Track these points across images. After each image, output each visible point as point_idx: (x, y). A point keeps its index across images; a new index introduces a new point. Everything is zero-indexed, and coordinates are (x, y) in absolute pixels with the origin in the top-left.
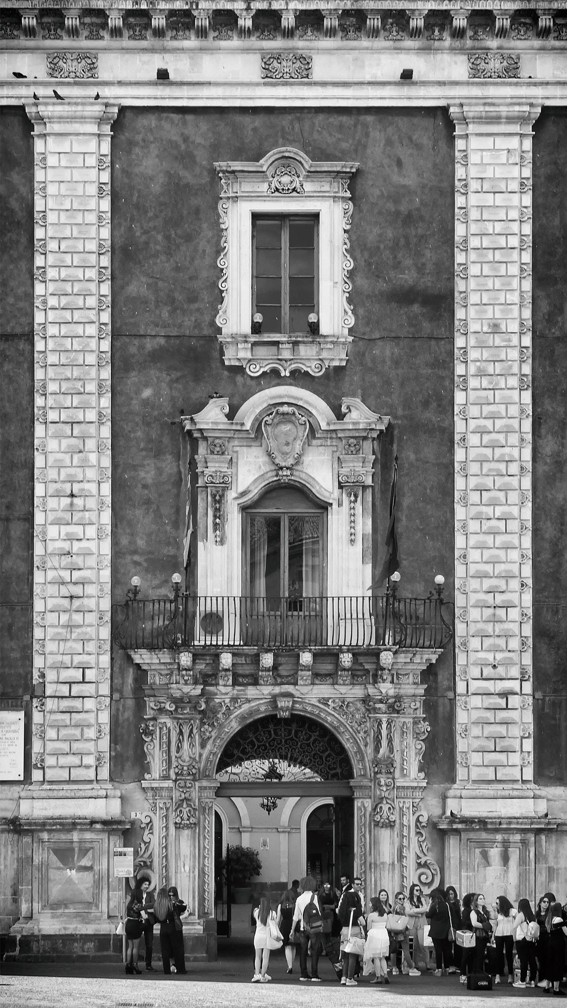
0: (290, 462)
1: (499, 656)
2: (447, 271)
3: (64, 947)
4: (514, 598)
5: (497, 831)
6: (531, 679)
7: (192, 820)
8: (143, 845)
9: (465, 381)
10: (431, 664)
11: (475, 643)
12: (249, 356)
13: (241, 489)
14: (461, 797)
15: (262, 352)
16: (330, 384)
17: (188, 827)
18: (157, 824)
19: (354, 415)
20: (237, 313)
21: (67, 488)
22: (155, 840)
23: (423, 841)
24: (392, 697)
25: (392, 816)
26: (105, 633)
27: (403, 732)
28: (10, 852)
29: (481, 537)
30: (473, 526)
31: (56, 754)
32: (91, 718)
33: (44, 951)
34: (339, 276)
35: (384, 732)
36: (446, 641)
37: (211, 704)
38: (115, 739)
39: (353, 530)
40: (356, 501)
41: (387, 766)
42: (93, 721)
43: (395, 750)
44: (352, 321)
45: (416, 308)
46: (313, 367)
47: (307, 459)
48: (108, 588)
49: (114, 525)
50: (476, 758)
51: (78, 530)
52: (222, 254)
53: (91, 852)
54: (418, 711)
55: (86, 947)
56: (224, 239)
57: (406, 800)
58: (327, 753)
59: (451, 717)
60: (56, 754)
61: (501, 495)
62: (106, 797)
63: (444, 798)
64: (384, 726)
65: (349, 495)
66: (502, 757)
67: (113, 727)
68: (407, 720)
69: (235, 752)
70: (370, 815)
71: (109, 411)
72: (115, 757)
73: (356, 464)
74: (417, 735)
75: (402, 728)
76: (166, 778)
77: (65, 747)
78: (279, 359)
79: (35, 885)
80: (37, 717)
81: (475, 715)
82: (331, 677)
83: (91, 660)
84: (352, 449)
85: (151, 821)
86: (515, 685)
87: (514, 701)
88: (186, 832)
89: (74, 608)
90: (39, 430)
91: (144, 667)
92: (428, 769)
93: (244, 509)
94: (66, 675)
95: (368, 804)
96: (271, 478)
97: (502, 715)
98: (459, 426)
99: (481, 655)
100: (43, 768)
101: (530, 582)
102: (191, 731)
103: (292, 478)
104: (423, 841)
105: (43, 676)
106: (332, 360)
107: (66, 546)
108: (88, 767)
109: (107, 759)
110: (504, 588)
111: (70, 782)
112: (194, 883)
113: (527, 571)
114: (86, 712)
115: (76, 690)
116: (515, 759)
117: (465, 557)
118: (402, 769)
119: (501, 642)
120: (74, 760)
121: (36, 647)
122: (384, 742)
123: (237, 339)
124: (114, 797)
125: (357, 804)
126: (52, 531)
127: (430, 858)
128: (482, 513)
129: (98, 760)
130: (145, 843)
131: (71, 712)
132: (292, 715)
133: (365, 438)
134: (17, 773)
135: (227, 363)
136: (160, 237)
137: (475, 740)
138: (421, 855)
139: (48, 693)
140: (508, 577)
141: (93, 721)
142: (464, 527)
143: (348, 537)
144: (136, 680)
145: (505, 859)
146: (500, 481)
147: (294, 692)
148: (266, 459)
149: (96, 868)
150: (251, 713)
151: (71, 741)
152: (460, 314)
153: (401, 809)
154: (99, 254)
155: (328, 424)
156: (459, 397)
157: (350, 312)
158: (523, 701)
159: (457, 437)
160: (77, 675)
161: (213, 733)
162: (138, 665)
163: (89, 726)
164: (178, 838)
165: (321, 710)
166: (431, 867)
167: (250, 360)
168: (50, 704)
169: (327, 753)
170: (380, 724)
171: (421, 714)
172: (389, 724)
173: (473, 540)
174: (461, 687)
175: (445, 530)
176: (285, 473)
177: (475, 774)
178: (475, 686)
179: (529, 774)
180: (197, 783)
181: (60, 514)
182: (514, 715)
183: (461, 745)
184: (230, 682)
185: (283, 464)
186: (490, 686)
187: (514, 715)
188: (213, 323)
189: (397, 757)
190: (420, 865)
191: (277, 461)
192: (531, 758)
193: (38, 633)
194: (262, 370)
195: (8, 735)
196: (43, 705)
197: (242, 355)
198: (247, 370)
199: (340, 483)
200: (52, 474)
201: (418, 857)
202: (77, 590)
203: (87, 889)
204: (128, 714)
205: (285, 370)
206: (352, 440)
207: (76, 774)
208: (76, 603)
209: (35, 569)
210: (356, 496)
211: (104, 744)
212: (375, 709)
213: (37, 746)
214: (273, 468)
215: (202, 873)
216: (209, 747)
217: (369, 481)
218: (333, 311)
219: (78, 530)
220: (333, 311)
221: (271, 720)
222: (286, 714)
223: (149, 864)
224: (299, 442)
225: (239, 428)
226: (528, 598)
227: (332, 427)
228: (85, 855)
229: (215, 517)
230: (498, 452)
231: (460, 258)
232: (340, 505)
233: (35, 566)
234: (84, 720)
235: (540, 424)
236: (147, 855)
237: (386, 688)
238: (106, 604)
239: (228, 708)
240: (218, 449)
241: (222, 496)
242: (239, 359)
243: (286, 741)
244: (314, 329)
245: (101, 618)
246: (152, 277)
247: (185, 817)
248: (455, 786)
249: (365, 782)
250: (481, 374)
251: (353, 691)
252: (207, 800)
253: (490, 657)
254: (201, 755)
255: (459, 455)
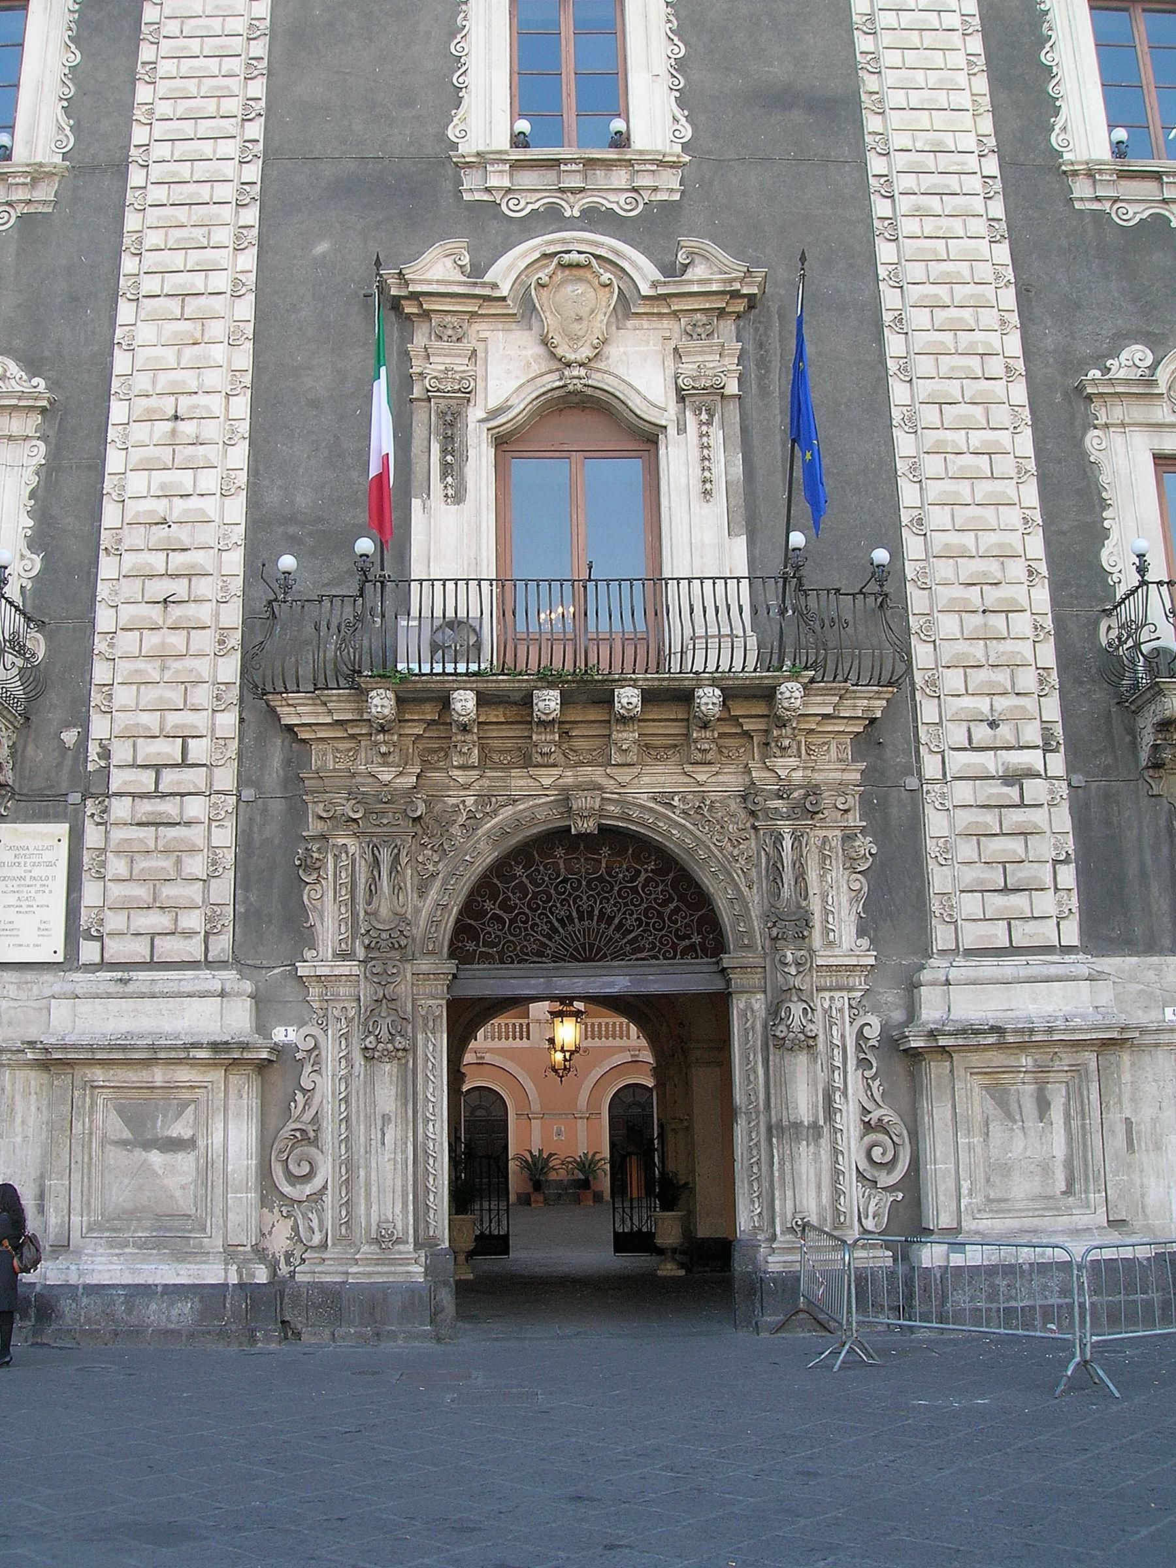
0: (585, 352)
1: (1001, 703)
2: (848, 66)
3: (129, 1311)
4: (1019, 594)
5: (1022, 1047)
6: (1062, 749)
7: (400, 1042)
8: (299, 1096)
9: (894, 226)
10: (873, 721)
11: (952, 680)
12: (506, 183)
13: (493, 404)
14: (948, 983)
15: (528, 179)
16: (655, 227)
17: (390, 1056)
18: (331, 1050)
19: (699, 271)
20: (485, 116)
21: (168, 406)
22: (325, 1085)
23: (873, 1078)
24: (801, 787)
25: (810, 1026)
26: (230, 669)
27: (825, 857)
28: (33, 1109)
29: (948, 485)
30: (932, 465)
31: (127, 907)
32: (195, 835)
33: (89, 1321)
34: (662, 66)
35: (788, 855)
36: (897, 677)
37: (438, 808)
38: (244, 881)
39: (707, 474)
40: (709, 423)
41: (790, 925)
42: (200, 842)
43: (811, 893)
44: (687, 133)
45: (797, 116)
46: (622, 202)
47: (613, 351)
48: (237, 585)
49: (254, 472)
50: (970, 905)
51: (185, 479)
52: (459, 37)
53: (193, 1106)
54: (850, 815)
55: (175, 1312)
56: (462, 15)
57: (837, 994)
58: (672, 906)
59: (915, 825)
60: (127, 907)
61: (978, 411)
62: (222, 994)
63: (912, 987)
64: (787, 843)
65: (697, 411)
66: (1018, 901)
67: (240, 856)
68: (829, 834)
69: (488, 905)
70: (765, 1027)
71: (253, 277)
72: (246, 915)
73: (708, 358)
74: (851, 863)
75: (821, 849)
76: (343, 956)
77: (141, 892)
78: (561, 190)
79: (76, 1177)
80: (93, 836)
81: (964, 818)
82: (680, 748)
83: (199, 721)
84: (699, 330)
85: (316, 1047)
86: (1034, 759)
87: (1035, 789)
88: (388, 1068)
89: (169, 623)
90: (125, 312)
91: (304, 735)
92: (875, 930)
93: (502, 442)
94: (150, 750)
95: (759, 1003)
96: (552, 381)
97: (1015, 817)
98: (890, 298)
99: (967, 702)
100: (100, 938)
101: (1043, 568)
102: (396, 860)
103: (590, 382)
104: (873, 1078)
105: (105, 754)
106: (655, 189)
107: (160, 507)
108: (189, 934)
109: (228, 920)
110: (999, 576)
111: (152, 965)
112: (405, 1175)
113: (1036, 546)
114: (188, 824)
115: (169, 779)
116: (1046, 903)
117: (920, 521)
118: (827, 931)
119: (1002, 677)
120: (157, 921)
121: (96, 698)
122: (788, 876)
123: (483, 160)
124: (239, 994)
125: (738, 1004)
126: (137, 483)
127: (884, 1113)
128: (946, 441)
129: (209, 920)
130: (304, 1091)
131: (157, 824)
132: (602, 829)
133: (722, 313)
134: (52, 948)
135: (467, 197)
136: (353, 16)
137: (964, 868)
138: (869, 1106)
139: (113, 788)
140: (1004, 556)
141: (200, 842)
142: (913, 468)
143: (696, 488)
144: (287, 762)
145: (1043, 1105)
146: (972, 388)
147: (604, 781)
148: (540, 350)
149: (201, 1143)
150: (517, 823)
151: (158, 881)
152: (873, 123)
153: (827, 1012)
154: (248, 39)
155: (654, 285)
156: (885, 252)
157: (683, 120)
158: (1051, 792)
159: (887, 317)
160: (171, 750)
161: (441, 866)
162: (290, 728)
163: (193, 851)
164: (370, 1082)
165: (659, 816)
166: (891, 1130)
167: (509, 190)
168: (120, 809)
169: (672, 906)
170: (779, 839)
171: (854, 820)
172: (796, 839)
173: (934, 490)
174: (931, 766)
175: (883, 474)
176: (575, 373)
177: (971, 936)
178: (959, 761)
179: (1071, 934)
180: (408, 966)
181: (153, 452)
182: (1037, 817)
183: (939, 879)
184: (474, 759)
185: (571, 357)
186: (988, 762)
187: (1037, 817)
188: (442, 137)
189: (815, 905)
190: (868, 1127)
191: (559, 352)
192: (1074, 903)
193: (101, 672)
194: (530, 207)
195: (36, 872)
196: (104, 812)
197: (493, 181)
198: (504, 207)
199: (679, 390)
200: (142, 382)
201: (866, 1112)
202: (180, 588)
203: (183, 1187)
204: (272, 830)
205: (572, 207)
206: (698, 316)
207: (169, 948)
208: (175, 612)
209: (102, 554)
210: (711, 416)
211: (223, 889)
212: (766, 810)
213: (91, 893)
214: (555, 365)
215: (420, 1154)
216: (433, 894)
217: (733, 388)
218: (653, 116)
219: (185, 479)
220: (653, 116)
221: (558, 837)
222: (588, 826)
223: (312, 1134)
224: (600, 316)
225: (487, 292)
226: (1042, 596)
227: (662, 290)
228: (180, 1114)
229: (444, 452)
230: (965, 338)
231: (864, 43)
232: (682, 430)
233: (102, 547)
234: (183, 840)
235: (1029, 300)
236: (309, 1116)
237: (788, 767)
238: (232, 615)
239: (471, 816)
240: (450, 332)
241: (457, 415)
242: (488, 190)
243: (588, 885)
244: (621, 141)
245: (221, 642)
246: (337, 72)
247: (384, 1035)
248: (933, 962)
249: (750, 958)
250: (920, 214)
251: (721, 778)
252: (430, 1002)
253: (982, 705)
254: (417, 911)
255: (894, 344)
